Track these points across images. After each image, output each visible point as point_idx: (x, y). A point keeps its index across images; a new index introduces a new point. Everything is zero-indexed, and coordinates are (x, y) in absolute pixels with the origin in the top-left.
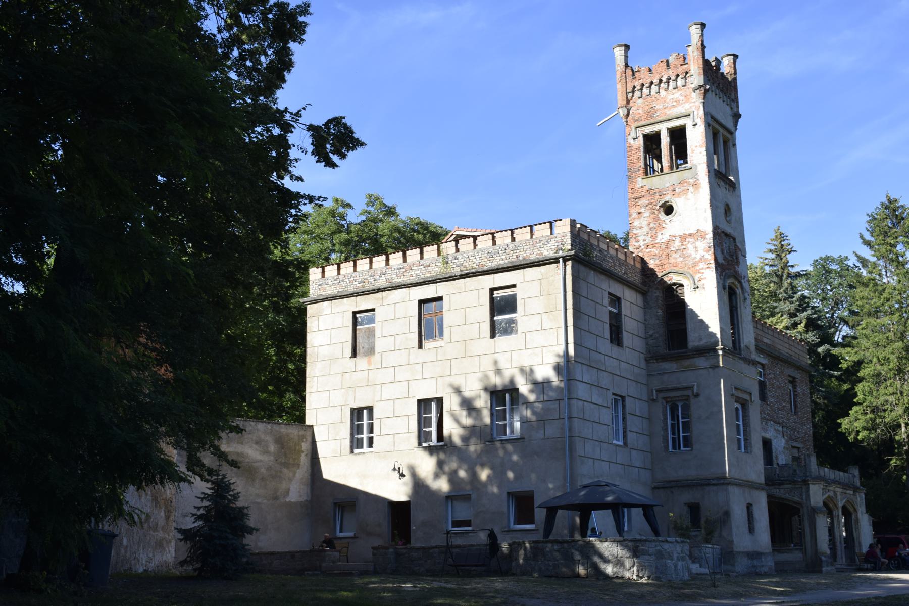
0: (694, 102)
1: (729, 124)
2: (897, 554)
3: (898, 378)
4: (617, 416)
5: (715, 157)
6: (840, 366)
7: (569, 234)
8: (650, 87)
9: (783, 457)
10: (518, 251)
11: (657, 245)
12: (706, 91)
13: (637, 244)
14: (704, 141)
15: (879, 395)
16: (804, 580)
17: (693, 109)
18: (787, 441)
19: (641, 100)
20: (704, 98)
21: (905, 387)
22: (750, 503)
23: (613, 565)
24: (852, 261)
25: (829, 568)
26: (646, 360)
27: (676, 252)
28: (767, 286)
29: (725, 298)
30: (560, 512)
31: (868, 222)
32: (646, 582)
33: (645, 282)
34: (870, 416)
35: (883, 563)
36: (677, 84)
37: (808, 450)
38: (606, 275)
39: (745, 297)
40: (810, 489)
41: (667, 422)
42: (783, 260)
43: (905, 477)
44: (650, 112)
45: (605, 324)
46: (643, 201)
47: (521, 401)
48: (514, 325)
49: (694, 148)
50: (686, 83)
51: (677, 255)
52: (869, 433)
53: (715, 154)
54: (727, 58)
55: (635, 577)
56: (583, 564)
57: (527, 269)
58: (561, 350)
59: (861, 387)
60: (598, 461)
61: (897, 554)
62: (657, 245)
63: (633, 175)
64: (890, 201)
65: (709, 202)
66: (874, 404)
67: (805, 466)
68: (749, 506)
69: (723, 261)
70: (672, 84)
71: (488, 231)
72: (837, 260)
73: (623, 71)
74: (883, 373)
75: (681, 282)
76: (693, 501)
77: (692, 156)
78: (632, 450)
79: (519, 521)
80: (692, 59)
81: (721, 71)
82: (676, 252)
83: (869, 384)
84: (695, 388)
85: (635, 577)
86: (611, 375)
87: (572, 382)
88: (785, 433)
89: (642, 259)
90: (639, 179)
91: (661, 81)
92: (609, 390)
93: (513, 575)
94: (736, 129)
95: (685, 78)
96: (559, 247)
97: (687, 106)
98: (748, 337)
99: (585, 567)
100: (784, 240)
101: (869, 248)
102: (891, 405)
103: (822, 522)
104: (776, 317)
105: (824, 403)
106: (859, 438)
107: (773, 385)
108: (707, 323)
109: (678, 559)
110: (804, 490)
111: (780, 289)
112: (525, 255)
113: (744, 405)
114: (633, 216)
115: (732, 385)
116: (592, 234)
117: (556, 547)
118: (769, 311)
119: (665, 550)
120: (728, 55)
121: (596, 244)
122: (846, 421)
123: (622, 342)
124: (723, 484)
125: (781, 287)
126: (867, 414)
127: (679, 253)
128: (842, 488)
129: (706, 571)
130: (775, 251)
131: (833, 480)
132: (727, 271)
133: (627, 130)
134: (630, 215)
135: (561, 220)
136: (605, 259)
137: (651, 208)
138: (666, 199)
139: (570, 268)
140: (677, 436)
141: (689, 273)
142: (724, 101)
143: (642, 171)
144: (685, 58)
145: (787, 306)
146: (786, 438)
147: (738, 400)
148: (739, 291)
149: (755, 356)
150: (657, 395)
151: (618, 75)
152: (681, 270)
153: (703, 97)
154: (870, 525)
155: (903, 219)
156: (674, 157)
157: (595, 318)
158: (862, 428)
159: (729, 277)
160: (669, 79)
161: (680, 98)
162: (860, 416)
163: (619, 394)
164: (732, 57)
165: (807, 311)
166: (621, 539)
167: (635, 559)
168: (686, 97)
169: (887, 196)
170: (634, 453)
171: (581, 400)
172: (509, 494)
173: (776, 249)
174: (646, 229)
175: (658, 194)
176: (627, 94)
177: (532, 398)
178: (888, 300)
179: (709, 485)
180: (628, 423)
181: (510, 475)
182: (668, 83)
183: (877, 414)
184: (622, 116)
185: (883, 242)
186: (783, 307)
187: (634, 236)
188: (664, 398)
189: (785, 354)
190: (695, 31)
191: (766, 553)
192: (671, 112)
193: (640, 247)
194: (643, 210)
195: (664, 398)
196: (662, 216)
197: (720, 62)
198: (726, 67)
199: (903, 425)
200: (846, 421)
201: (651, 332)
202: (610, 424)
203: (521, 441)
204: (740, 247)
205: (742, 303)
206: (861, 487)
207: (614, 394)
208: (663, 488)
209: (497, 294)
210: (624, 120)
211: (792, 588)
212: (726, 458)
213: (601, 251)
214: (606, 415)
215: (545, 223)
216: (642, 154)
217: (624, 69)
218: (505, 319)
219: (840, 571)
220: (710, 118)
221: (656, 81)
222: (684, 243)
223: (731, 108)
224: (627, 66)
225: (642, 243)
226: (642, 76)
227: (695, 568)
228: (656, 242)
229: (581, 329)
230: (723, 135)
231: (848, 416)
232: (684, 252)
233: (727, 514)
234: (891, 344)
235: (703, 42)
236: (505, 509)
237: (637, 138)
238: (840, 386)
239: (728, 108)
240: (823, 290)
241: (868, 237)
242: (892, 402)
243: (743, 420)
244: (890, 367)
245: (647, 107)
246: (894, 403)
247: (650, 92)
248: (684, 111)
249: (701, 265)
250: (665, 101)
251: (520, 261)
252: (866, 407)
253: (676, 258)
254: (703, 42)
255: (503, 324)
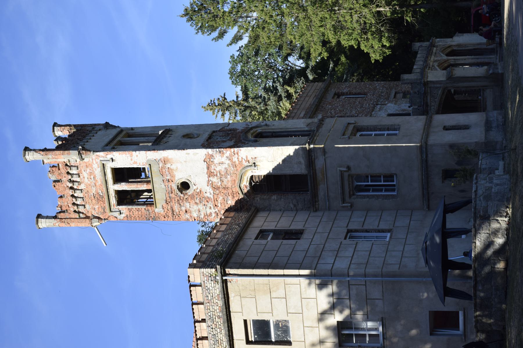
0: (92, 159)
1: (114, 132)
2: (487, 15)
3: (338, 12)
4: (365, 237)
5: (141, 144)
6: (326, 58)
7: (202, 270)
8: (76, 198)
9: (403, 105)
10: (214, 317)
11: (215, 198)
12: (84, 149)
13: (214, 215)
14: (127, 152)
15: (352, 27)
16: (510, 82)
17: (98, 161)
18: (389, 102)
19: (87, 206)
20: (90, 151)
21: (346, 6)
22: (443, 127)
23: (496, 237)
24: (234, 50)
25: (500, 67)
26: (316, 211)
27: (222, 181)
28: (254, 116)
29: (264, 141)
30: (449, 285)
31: (203, 33)
32: (511, 210)
33: (247, 209)
34: (369, 36)
35: (495, 25)
36: (75, 174)
37: (397, 85)
38: (239, 241)
39: (264, 125)
40: (431, 80)
41: (371, 195)
42: (232, 104)
43: (422, 10)
44: (98, 198)
45: (283, 243)
46: (176, 208)
47: (350, 320)
48: (280, 324)
49: (133, 161)
50: (75, 166)
51: (225, 180)
52: (384, 37)
53: (139, 145)
54: (56, 132)
55: (507, 219)
56: (495, 264)
57: (231, 309)
58: (304, 282)
59: (344, 41)
60: (404, 253)
61: (487, 15)
62: (215, 198)
63: (152, 215)
64: (186, 14)
65: (180, 151)
66: (359, 31)
67: (411, 84)
68: (446, 128)
69: (233, 141)
70: (75, 178)
71: (194, 344)
72: (233, 65)
73: (60, 221)
74: (333, 23)
75: (249, 178)
76: (441, 175)
77: (140, 163)
78: (395, 226)
79: (457, 327)
80: (54, 160)
81: (67, 137)
82: (222, 181)
83: (342, 35)
84: (342, 169)
85: (507, 219)
86: (328, 240)
87: (333, 273)
88: (383, 103)
89: (227, 211)
90: (156, 210)
91: (71, 188)
92: (341, 242)
93: (504, 328)
94: (118, 127)
95: (70, 167)
96: (212, 279)
97: (95, 166)
98: (300, 124)
99: (498, 262)
100: (214, 103)
101: (225, 34)
102: (360, 18)
103: (459, 72)
104: (281, 110)
105: (357, 76)
106: (388, 45)
107: (340, 111)
108: (285, 157)
109: (492, 182)
110: (432, 86)
111: (257, 108)
112: (218, 311)
113: (358, 129)
114: (189, 217)
115: (341, 138)
116: (203, 250)
117: (480, 288)
118: (276, 116)
119: (483, 193)
120: (54, 131)
121: (212, 248)
122: (373, 55)
123: (300, 230)
124: (426, 149)
125: (255, 108)
126: (367, 38)
127: (223, 178)
128: (431, 55)
129: (501, 163)
130: (223, 111)
131: (424, 62)
132: (242, 139)
133: (112, 219)
134: (188, 220)
135: (189, 277)
136: (226, 241)
137: (183, 201)
138: (175, 187)
139: (232, 270)
140: (384, 188)
141: (241, 170)
142: (93, 136)
143: (149, 208)
144: (53, 166)
145: (272, 104)
146: (386, 102)
147: (354, 134)
148: (259, 130)
149: (316, 120)
150: (347, 203)
151: (63, 225)
152: (239, 177)
153: (88, 152)
154: (463, 35)
155: (202, 4)
156: (138, 180)
157: (277, 251)
158: (379, 42)
159: (247, 137)
160: (70, 181)
161: (87, 172)
162: (370, 44)
163: (345, 234)
164: (55, 128)
165: (277, 86)
166: (473, 230)
167: (491, 219)
168: (87, 166)
169: (182, 17)
170: (397, 224)
171: (350, 265)
172: (431, 334)
173: (222, 110)
174: (201, 207)
175: (171, 195)
176: (80, 218)
177: (347, 312)
178: (271, 16)
179: (426, 161)
180: (371, 228)
181: (414, 332)
182: (73, 181)
183: (368, 30)
184: (99, 223)
185: (221, 19)
186: (272, 107)
187: (206, 217)
188: (350, 197)
189: (314, 100)
190: (31, 156)
191: (486, 116)
192: (99, 180)
193: (216, 212)
194: (183, 209)
195: (350, 197)
196: (190, 192)
197: (59, 137)
198: (64, 133)
199: (378, 9)
200: (373, 55)
201: (292, 206)
202: (372, 242)
203: (384, 321)
204: (221, 127)
205: (270, 128)
206: (431, 41)
207: (345, 238)
208: (429, 200)
209: (252, 338)
210: (103, 222)
211: (516, 90)
212: (404, 145)
213: (218, 244)
214: (364, 245)
215: (191, 291)
216: (134, 207)
217: (58, 220)
218: (275, 331)
219: (502, 59)
220: (107, 147)
221: (71, 192)
222: (215, 173)
223: (100, 130)
224: (55, 217)
225: (213, 211)
226: (66, 204)
227: (499, 172)
228: (212, 198)
229: (287, 263)
230: (123, 137)
231: (369, 53)
232: (223, 174)
233: (452, 146)
234: (309, 15)
235: (40, 150)
236: (446, 338)
237: (120, 211)
238: (342, 64)
239: (99, 133)
240: (258, 78)
241: (215, 34)
242: (358, 17)
243: (371, 131)
244: (328, 17)
245: (94, 201)
246: (359, 15)
247: (80, 198)
248: (99, 168)
249: (235, 159)
250: (90, 185)
251: (223, 315)
252: (362, 38)
253: (228, 181)
254: (40, 150)
255: (279, 333)
